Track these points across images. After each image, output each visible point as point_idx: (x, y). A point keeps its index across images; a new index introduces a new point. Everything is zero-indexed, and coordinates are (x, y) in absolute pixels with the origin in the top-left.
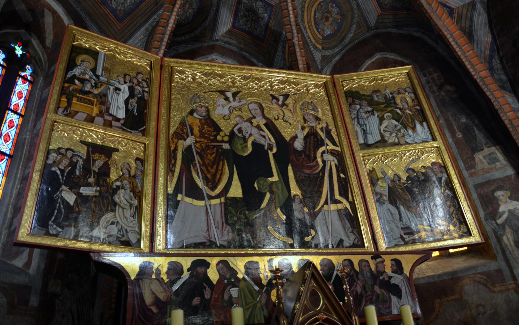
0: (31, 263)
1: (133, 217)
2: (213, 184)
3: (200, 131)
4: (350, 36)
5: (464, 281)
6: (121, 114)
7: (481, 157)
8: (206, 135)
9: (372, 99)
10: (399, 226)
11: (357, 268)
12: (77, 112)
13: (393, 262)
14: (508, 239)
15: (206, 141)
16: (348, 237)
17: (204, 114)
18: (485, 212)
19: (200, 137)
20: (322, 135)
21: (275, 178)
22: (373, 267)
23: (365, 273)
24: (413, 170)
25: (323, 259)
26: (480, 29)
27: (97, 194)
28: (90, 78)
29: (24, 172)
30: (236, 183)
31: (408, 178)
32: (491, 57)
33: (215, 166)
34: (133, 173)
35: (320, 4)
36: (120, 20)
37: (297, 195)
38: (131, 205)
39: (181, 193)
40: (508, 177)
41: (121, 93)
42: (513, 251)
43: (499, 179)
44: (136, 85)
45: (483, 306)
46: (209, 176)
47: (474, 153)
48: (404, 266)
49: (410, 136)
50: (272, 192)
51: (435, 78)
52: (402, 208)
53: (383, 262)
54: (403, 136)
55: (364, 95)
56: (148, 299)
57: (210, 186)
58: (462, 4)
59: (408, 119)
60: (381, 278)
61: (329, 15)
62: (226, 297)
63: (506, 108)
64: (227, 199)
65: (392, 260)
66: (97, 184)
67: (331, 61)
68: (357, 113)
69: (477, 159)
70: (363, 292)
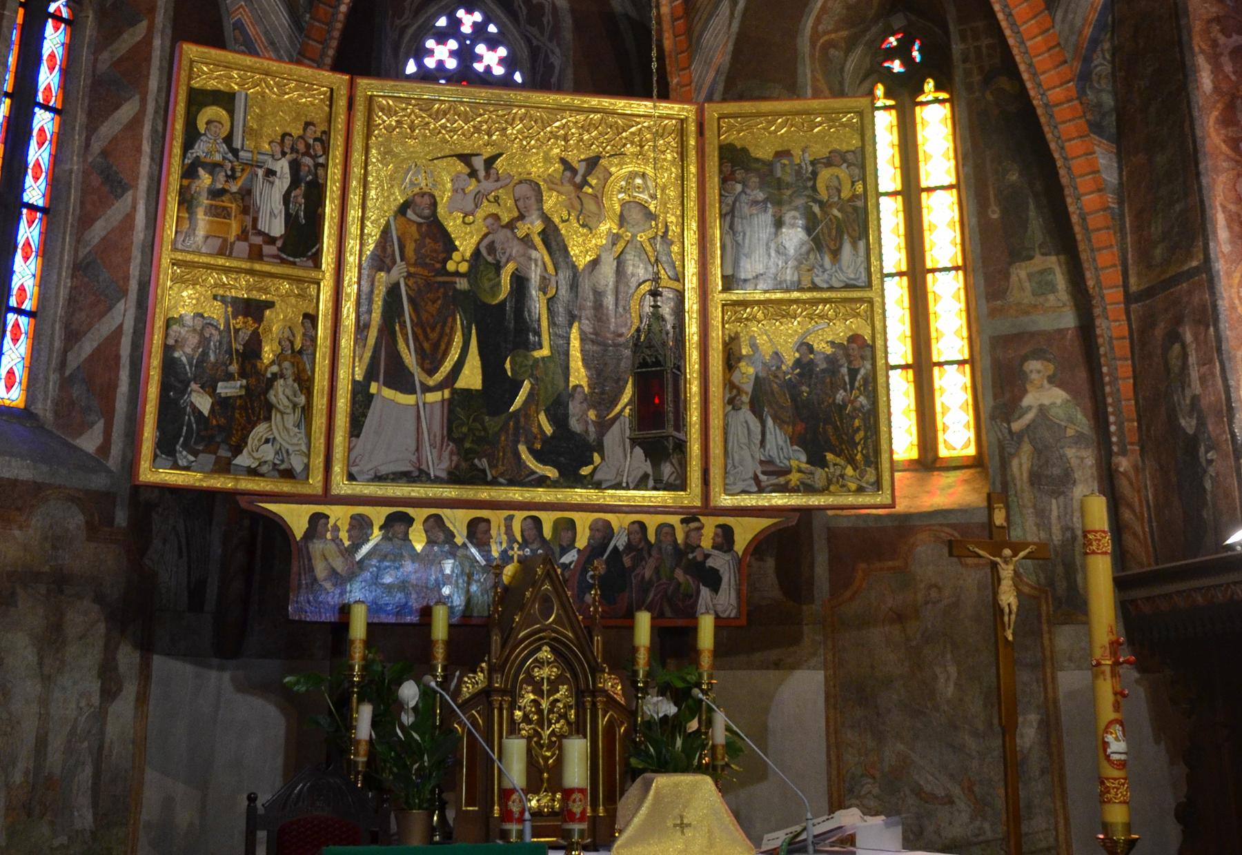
0: (110, 449)
1: (298, 426)
3: (416, 251)
5: (919, 537)
6: (277, 228)
7: (1023, 274)
8: (428, 261)
9: (771, 172)
10: (757, 456)
11: (652, 537)
13: (719, 530)
14: (1021, 465)
15: (426, 273)
17: (427, 212)
18: (995, 399)
19: (415, 265)
22: (680, 537)
23: (664, 546)
25: (596, 521)
27: (243, 393)
28: (224, 158)
29: (76, 251)
31: (798, 363)
32: (1095, 42)
33: (439, 327)
34: (298, 346)
37: (581, 386)
38: (295, 406)
39: (377, 380)
40: (1061, 332)
41: (277, 181)
42: (1023, 491)
44: (304, 154)
45: (940, 589)
46: (426, 345)
47: (1010, 264)
48: (737, 537)
49: (824, 271)
50: (537, 381)
51: (984, 50)
52: (770, 422)
53: (702, 527)
55: (757, 160)
57: (427, 365)
59: (830, 230)
60: (691, 556)
63: (1084, 183)
64: (454, 392)
65: (718, 526)
66: (243, 374)
68: (734, 203)
69: (1014, 278)
70: (654, 578)
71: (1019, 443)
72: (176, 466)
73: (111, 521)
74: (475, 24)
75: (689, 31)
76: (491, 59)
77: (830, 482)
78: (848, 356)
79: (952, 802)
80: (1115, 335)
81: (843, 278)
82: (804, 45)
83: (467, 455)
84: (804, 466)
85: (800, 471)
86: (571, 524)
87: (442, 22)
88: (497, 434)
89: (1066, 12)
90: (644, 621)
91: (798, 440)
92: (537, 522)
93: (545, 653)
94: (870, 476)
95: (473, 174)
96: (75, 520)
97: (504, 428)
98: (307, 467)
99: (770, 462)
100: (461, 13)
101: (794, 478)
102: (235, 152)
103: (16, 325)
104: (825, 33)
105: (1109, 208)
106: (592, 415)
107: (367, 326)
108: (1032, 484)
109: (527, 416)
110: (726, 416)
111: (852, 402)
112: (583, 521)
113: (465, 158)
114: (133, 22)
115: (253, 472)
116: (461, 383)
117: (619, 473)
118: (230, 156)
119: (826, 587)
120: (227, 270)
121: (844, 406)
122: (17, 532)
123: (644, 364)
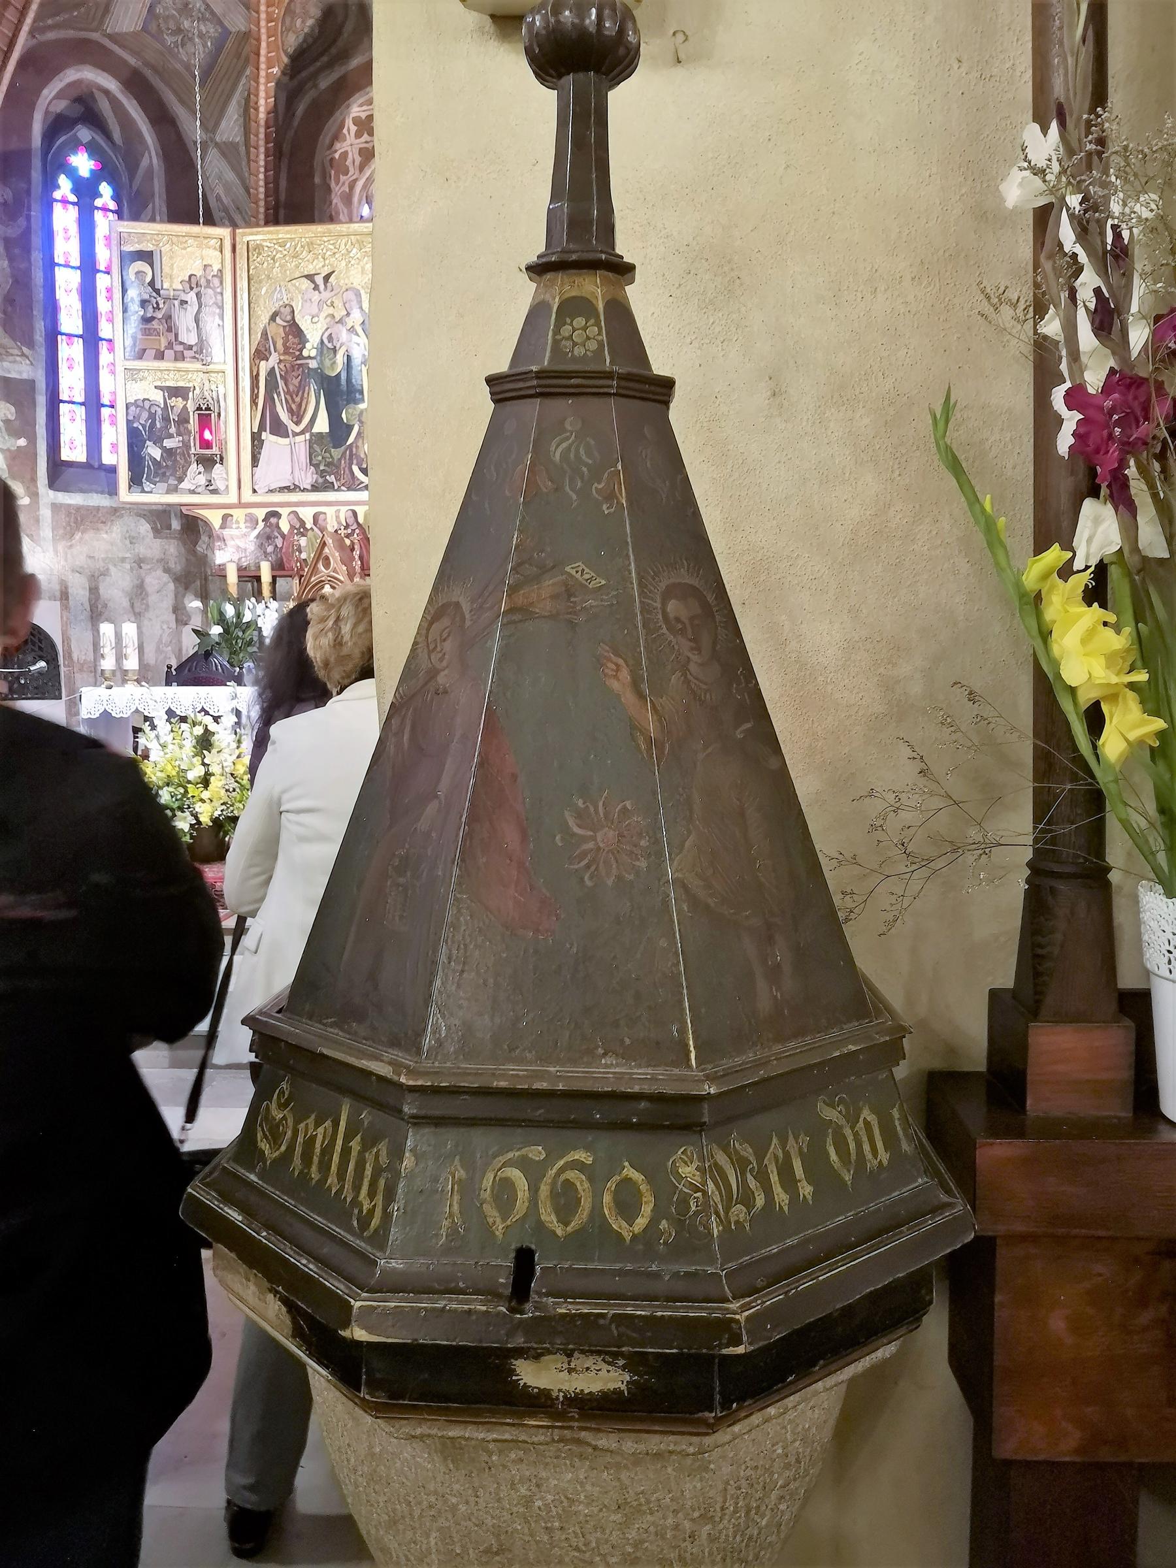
2: (297, 416)
3: (284, 345)
19: (285, 353)
30: (323, 416)
46: (294, 406)
57: (295, 419)
72: (143, 491)
73: (169, 527)
83: (322, 474)
88: (340, 460)
92: (355, 513)
95: (316, 288)
97: (344, 453)
102: (157, 292)
107: (257, 397)
109: (357, 447)
113: (310, 277)
115: (193, 492)
116: (315, 430)
118: (154, 294)
122: (105, 536)
123: (199, 408)
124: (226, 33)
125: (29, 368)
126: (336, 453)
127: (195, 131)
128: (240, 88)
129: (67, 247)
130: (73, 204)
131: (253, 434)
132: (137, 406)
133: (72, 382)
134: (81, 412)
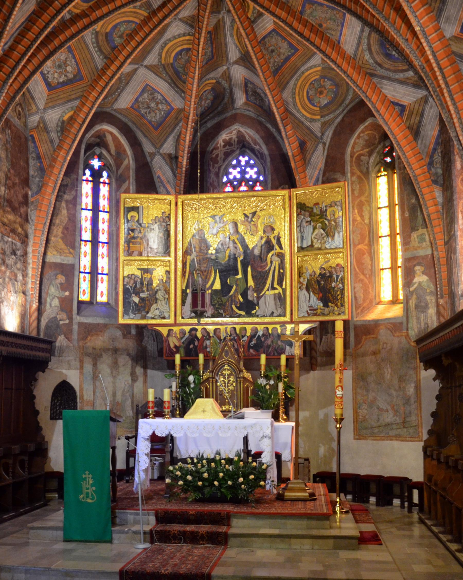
4: (349, 97)
7: (415, 236)
9: (312, 211)
11: (270, 332)
12: (133, 252)
16: (277, 310)
20: (274, 242)
21: (240, 276)
22: (279, 331)
24: (324, 269)
25: (253, 327)
26: (429, 124)
31: (320, 274)
32: (435, 150)
35: (311, 83)
36: (156, 129)
38: (165, 298)
43: (420, 257)
45: (387, 344)
47: (412, 232)
50: (237, 285)
52: (311, 294)
54: (325, 243)
55: (308, 207)
56: (172, 346)
58: (415, 100)
61: (323, 89)
62: (204, 345)
66: (148, 290)
67: (333, 122)
69: (412, 237)
71: (412, 295)
72: (130, 318)
73: (130, 333)
74: (246, 161)
75: (304, 159)
76: (252, 173)
77: (330, 312)
78: (336, 271)
79: (388, 411)
80: (441, 256)
81: (335, 245)
82: (348, 157)
83: (217, 309)
84: (322, 307)
85: (321, 309)
86: (245, 329)
87: (234, 162)
88: (226, 302)
89: (422, 140)
90: (263, 357)
91: (321, 299)
92: (235, 329)
93: (226, 367)
94: (342, 310)
96: (119, 333)
97: (228, 300)
98: (169, 316)
99: (312, 306)
100: (241, 158)
101: (319, 311)
103: (102, 278)
104: (357, 152)
105: (439, 211)
106: (255, 295)
107: (185, 272)
108: (416, 308)
109: (235, 296)
110: (298, 292)
111: (337, 286)
112: (249, 328)
114: (124, 182)
115: (153, 318)
117: (264, 312)
119: (353, 344)
120: (141, 261)
121: (335, 287)
122: (101, 338)
124: (172, 109)
125: (73, 259)
126: (224, 299)
127: (148, 148)
128: (176, 131)
129: (87, 201)
130: (91, 181)
131: (182, 290)
132: (129, 278)
133: (85, 262)
134: (88, 277)
